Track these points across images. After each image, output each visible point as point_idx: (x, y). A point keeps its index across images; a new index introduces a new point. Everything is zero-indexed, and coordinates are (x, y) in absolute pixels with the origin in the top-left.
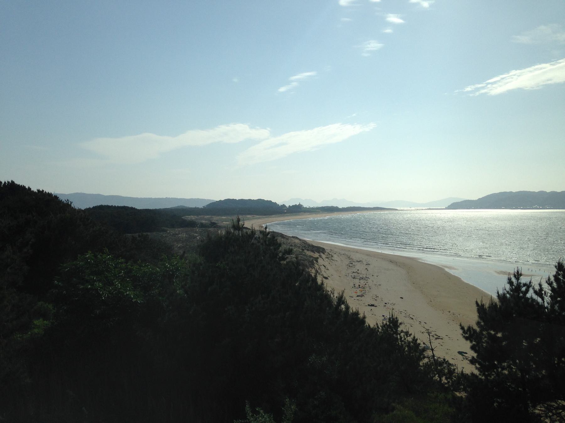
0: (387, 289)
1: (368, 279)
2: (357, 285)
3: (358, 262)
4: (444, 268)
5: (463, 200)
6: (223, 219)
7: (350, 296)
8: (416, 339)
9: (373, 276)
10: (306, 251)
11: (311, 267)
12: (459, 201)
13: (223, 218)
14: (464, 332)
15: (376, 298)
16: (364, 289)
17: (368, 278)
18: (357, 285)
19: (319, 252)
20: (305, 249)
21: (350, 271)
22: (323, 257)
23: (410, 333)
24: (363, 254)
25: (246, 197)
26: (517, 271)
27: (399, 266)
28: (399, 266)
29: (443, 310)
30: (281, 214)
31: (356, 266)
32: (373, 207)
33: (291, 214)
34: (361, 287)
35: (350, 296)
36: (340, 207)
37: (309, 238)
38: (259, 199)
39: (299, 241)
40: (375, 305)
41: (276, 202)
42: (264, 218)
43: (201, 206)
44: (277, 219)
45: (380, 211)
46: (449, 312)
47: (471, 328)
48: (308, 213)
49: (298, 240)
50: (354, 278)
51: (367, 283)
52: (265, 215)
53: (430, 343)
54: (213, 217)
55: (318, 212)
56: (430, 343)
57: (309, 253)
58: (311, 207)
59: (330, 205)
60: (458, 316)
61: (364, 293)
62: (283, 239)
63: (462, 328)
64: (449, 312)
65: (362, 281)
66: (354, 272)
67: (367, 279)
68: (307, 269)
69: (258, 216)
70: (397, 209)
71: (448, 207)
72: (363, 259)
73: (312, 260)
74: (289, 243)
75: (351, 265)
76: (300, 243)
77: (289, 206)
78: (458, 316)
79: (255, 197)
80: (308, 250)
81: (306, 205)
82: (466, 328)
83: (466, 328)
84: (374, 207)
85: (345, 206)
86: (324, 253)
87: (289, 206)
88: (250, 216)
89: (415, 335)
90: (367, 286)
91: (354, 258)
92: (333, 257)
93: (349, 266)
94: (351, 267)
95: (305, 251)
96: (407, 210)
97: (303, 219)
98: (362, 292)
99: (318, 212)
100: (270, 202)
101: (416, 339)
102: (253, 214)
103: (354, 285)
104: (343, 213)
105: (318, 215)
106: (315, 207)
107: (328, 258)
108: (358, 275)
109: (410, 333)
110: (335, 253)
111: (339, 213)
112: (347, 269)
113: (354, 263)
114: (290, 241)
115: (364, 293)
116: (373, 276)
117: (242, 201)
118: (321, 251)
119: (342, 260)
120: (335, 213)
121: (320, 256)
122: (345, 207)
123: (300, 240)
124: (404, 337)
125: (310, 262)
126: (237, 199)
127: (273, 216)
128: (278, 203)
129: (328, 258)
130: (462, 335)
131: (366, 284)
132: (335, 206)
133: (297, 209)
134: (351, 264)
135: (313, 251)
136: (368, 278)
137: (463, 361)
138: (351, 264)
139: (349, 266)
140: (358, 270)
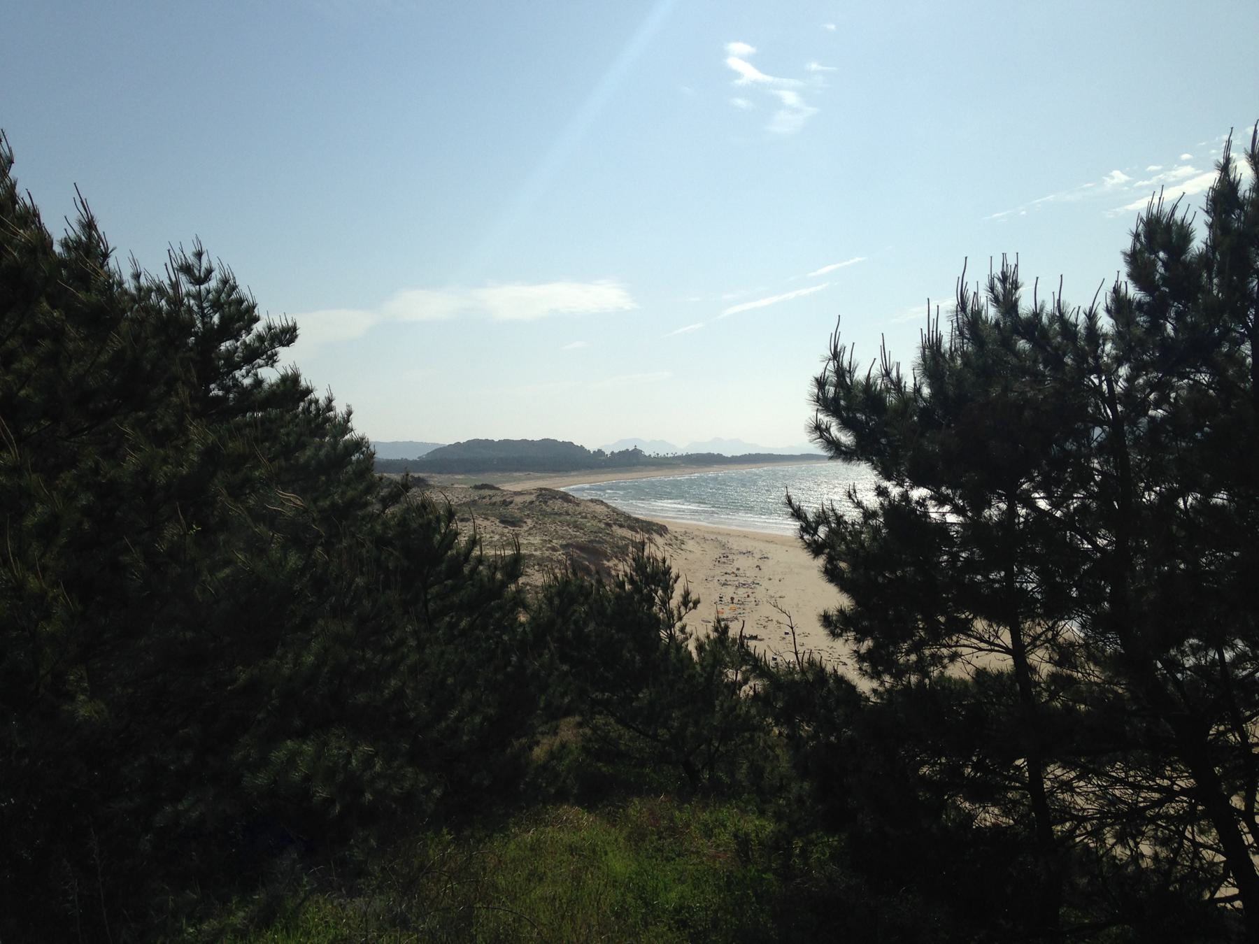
0: (798, 604)
1: (757, 586)
2: (727, 599)
3: (742, 555)
6: (456, 479)
7: (703, 621)
9: (770, 579)
10: (618, 527)
11: (616, 557)
13: (456, 477)
15: (764, 624)
16: (742, 606)
17: (758, 584)
18: (727, 599)
19: (648, 532)
20: (614, 524)
21: (718, 571)
22: (202, 261)
23: (693, 597)
24: (755, 538)
25: (516, 435)
30: (592, 468)
31: (735, 562)
33: (614, 469)
34: (735, 601)
35: (703, 621)
36: (728, 453)
37: (641, 509)
38: (545, 439)
39: (606, 509)
40: (759, 637)
41: (584, 446)
42: (551, 477)
43: (413, 456)
44: (579, 479)
48: (654, 467)
49: (603, 507)
50: (724, 584)
51: (751, 595)
52: (554, 471)
54: (433, 475)
57: (619, 532)
58: (661, 454)
61: (740, 614)
62: (565, 505)
65: (741, 591)
66: (726, 573)
67: (754, 585)
68: (605, 562)
69: (539, 475)
72: (755, 548)
73: (627, 545)
74: (580, 514)
75: (723, 560)
76: (607, 513)
77: (612, 453)
79: (535, 435)
80: (621, 526)
81: (648, 451)
86: (661, 535)
87: (612, 453)
88: (521, 474)
90: (752, 599)
91: (735, 547)
92: (683, 544)
93: (719, 561)
94: (724, 563)
95: (615, 528)
97: (693, 507)
98: (736, 612)
100: (570, 445)
102: (526, 470)
103: (720, 597)
104: (731, 467)
105: (676, 472)
106: (670, 455)
107: (670, 545)
108: (736, 579)
110: (693, 538)
112: (711, 567)
113: (731, 557)
114: (582, 508)
115: (740, 614)
116: (770, 579)
117: (506, 443)
118: (655, 531)
119: (705, 551)
121: (651, 540)
122: (739, 454)
123: (607, 506)
125: (618, 547)
126: (496, 440)
127: (573, 473)
128: (587, 447)
129: (670, 545)
131: (748, 596)
132: (716, 453)
133: (630, 460)
134: (725, 557)
135: (632, 528)
136: (758, 584)
137: (784, 638)
138: (725, 557)
139: (719, 561)
140: (738, 569)
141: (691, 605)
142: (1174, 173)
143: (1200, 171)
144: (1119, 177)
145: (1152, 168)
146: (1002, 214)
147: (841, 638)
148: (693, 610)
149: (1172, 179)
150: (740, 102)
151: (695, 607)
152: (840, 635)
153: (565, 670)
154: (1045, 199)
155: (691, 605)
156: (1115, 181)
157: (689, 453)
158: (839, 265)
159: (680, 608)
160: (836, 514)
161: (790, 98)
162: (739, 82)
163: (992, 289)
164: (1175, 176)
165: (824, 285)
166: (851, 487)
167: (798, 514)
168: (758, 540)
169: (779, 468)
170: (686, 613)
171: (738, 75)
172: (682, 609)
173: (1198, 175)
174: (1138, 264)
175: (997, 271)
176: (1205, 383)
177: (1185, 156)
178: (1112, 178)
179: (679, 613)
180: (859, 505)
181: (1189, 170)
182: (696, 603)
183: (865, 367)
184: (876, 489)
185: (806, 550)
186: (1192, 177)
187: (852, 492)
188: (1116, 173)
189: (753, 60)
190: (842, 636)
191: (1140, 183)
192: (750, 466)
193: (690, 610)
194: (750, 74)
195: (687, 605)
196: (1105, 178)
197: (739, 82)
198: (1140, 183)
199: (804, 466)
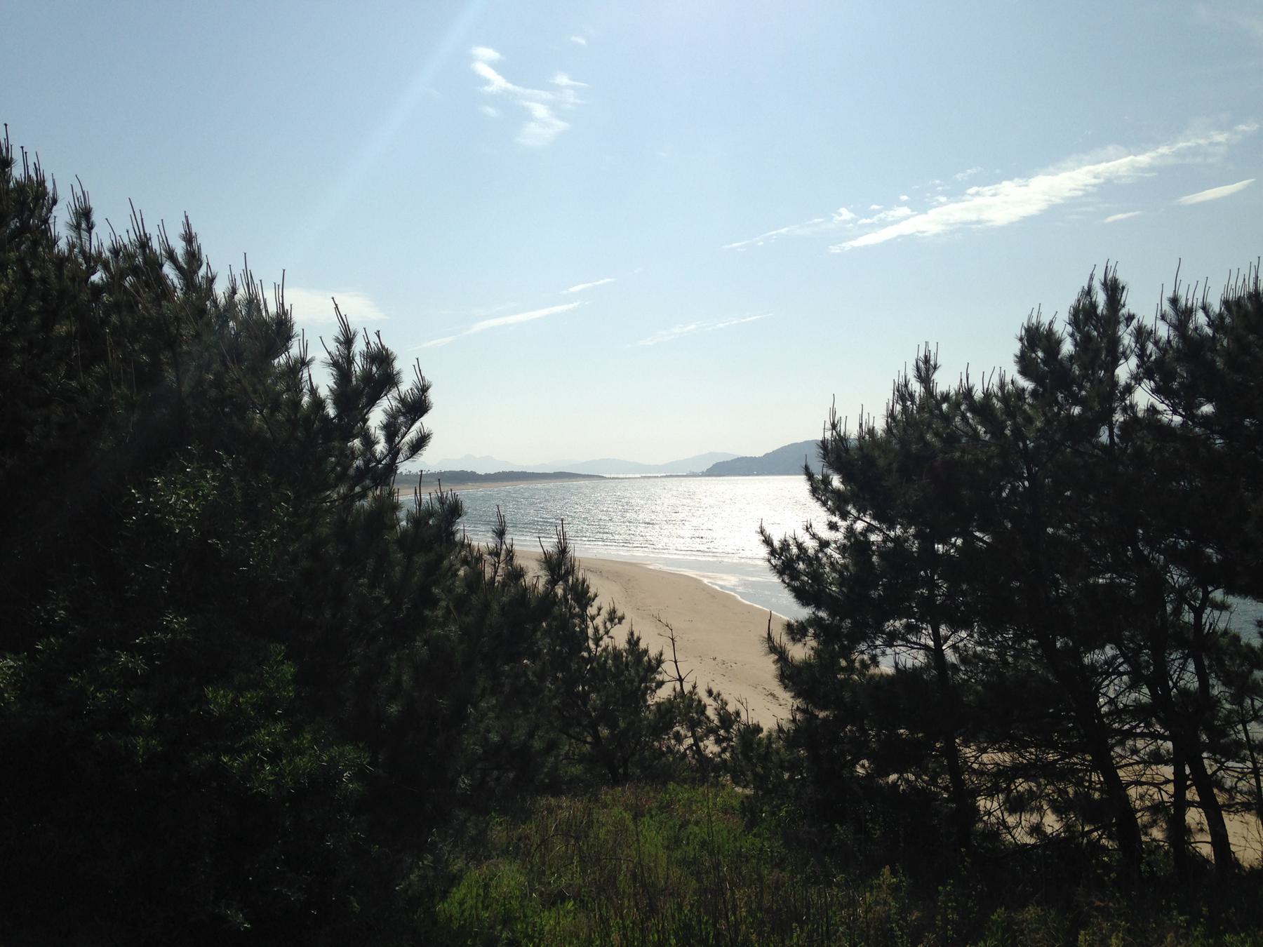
4: (701, 579)
5: (736, 457)
8: (635, 638)
12: (729, 459)
14: (773, 552)
23: (619, 614)
26: (926, 357)
27: (607, 577)
28: (607, 577)
29: (700, 657)
32: (552, 472)
36: (481, 471)
45: (567, 480)
46: (715, 659)
47: (791, 542)
48: (406, 485)
53: (676, 662)
55: (430, 482)
56: (676, 662)
59: (457, 468)
60: (734, 665)
63: (768, 542)
64: (715, 659)
70: (600, 477)
71: (706, 472)
78: (734, 665)
82: (777, 544)
83: (777, 544)
84: (555, 473)
85: (492, 470)
89: (633, 629)
96: (623, 478)
99: (430, 482)
101: (635, 638)
104: (485, 484)
109: (619, 614)
111: (478, 484)
120: (470, 484)
124: (606, 627)
130: (769, 561)
141: (616, 620)
142: (892, 213)
143: (916, 213)
144: (846, 214)
145: (874, 207)
146: (740, 244)
147: (800, 643)
148: (619, 625)
149: (890, 219)
150: (490, 111)
151: (620, 622)
152: (800, 640)
153: (963, 632)
154: (779, 231)
155: (616, 620)
156: (842, 218)
157: (443, 471)
158: (590, 285)
159: (605, 623)
160: (797, 542)
161: (540, 111)
162: (487, 89)
163: (918, 369)
164: (893, 216)
165: (575, 304)
166: (809, 522)
167: (768, 542)
168: (527, 558)
169: (540, 486)
170: (612, 627)
171: (487, 82)
172: (608, 625)
173: (912, 216)
174: (1025, 364)
175: (922, 355)
176: (1186, 481)
177: (904, 198)
178: (840, 215)
179: (606, 627)
180: (814, 536)
181: (905, 211)
182: (621, 619)
183: (852, 430)
184: (829, 524)
185: (772, 572)
186: (907, 218)
187: (809, 526)
188: (843, 210)
189: (495, 66)
190: (801, 641)
191: (864, 221)
192: (506, 483)
193: (615, 625)
194: (498, 83)
195: (613, 621)
196: (833, 215)
197: (487, 89)
198: (864, 221)
199: (559, 483)
